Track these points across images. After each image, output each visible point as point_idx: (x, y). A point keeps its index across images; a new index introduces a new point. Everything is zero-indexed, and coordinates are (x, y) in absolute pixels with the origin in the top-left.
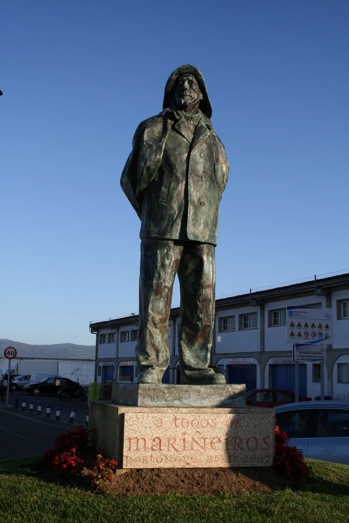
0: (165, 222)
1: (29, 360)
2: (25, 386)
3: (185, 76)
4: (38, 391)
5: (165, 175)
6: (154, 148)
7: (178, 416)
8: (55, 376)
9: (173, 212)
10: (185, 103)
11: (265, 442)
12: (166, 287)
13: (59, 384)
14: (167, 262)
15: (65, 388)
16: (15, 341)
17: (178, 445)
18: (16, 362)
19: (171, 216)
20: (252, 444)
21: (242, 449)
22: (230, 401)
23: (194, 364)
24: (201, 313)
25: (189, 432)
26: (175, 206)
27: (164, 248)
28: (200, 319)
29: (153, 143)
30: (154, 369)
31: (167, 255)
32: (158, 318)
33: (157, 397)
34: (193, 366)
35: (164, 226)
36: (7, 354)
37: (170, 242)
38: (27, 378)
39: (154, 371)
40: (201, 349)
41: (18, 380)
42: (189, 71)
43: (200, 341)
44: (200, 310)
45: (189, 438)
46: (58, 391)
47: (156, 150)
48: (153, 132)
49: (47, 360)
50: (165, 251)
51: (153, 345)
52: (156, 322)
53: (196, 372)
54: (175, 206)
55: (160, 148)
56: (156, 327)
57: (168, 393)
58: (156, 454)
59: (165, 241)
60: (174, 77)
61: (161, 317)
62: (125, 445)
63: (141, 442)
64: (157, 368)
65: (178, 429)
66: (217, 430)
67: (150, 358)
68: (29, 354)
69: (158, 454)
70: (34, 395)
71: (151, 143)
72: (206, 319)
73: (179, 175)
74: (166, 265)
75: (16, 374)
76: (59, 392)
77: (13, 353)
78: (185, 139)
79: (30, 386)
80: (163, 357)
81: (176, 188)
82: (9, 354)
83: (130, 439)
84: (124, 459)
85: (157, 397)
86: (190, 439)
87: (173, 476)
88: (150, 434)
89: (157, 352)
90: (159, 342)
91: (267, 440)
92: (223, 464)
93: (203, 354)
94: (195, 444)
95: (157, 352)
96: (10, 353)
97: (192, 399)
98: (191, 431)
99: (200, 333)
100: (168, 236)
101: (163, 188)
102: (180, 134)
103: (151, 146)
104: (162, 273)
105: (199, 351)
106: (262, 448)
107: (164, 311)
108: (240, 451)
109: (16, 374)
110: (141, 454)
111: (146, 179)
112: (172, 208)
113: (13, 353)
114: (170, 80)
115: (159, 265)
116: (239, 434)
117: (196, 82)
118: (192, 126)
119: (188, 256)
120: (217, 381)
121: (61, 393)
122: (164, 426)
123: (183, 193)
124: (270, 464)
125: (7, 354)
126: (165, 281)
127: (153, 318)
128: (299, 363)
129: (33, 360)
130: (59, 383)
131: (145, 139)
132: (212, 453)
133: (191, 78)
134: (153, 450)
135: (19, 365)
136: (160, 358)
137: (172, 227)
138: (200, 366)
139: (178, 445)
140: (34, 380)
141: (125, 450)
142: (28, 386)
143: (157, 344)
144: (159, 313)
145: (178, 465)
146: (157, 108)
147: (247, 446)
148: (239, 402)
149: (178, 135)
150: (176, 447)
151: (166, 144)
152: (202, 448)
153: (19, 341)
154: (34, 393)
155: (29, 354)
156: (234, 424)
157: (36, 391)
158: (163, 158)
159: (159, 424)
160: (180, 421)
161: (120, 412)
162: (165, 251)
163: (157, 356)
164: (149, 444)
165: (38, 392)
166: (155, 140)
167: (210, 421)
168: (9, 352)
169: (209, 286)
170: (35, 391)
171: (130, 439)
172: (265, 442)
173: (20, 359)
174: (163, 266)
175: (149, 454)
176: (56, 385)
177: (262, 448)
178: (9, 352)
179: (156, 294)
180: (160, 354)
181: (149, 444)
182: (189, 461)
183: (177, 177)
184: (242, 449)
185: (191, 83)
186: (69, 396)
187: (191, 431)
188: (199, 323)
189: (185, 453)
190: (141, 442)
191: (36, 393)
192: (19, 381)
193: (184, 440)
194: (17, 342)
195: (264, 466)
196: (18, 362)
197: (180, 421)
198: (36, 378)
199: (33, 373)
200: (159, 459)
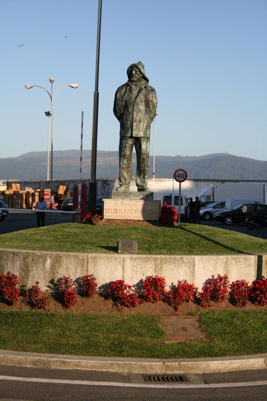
0: (126, 130)
1: (232, 183)
2: (215, 214)
3: (134, 68)
4: (230, 219)
5: (126, 111)
6: (121, 100)
7: (123, 202)
8: (255, 202)
9: (128, 126)
10: (133, 80)
11: (156, 212)
12: (127, 155)
13: (246, 211)
14: (127, 145)
15: (254, 216)
16: (239, 156)
17: (123, 211)
18: (212, 186)
19: (128, 128)
20: (150, 212)
21: (147, 214)
22: (146, 198)
23: (140, 184)
24: (142, 164)
25: (127, 207)
26: (129, 123)
27: (125, 140)
28: (141, 167)
29: (120, 98)
30: (122, 186)
31: (127, 143)
32: (124, 166)
33: (119, 196)
34: (139, 185)
35: (125, 131)
36: (177, 176)
37: (128, 137)
38: (223, 204)
39: (123, 187)
40: (143, 178)
41: (213, 208)
42: (134, 66)
43: (142, 175)
44: (141, 163)
45: (127, 209)
46: (246, 219)
47: (121, 101)
48: (121, 93)
49: (255, 183)
50: (126, 141)
51: (123, 177)
52: (124, 168)
53: (141, 187)
54: (129, 123)
55: (123, 100)
56: (124, 170)
57: (123, 194)
58: (115, 214)
59: (126, 137)
60: (129, 69)
61: (126, 166)
62: (104, 211)
63: (110, 210)
64: (124, 186)
65: (123, 206)
66: (137, 207)
67: (122, 182)
68: (260, 175)
69: (116, 214)
70: (225, 224)
71: (120, 98)
72: (144, 167)
73: (130, 111)
74: (126, 146)
75: (212, 201)
76: (247, 220)
77: (183, 176)
78: (134, 95)
79: (221, 214)
80: (128, 181)
81: (129, 116)
82: (179, 177)
83: (106, 209)
84: (104, 215)
85: (119, 196)
86: (127, 210)
87: (120, 222)
88: (113, 207)
89: (125, 179)
90: (126, 176)
91: (156, 211)
92: (141, 218)
93: (144, 180)
94: (129, 212)
95: (125, 179)
96: (180, 176)
97: (132, 197)
98: (127, 207)
99: (142, 172)
100: (126, 135)
101: (124, 116)
102: (132, 93)
103: (120, 100)
104: (125, 149)
105: (142, 179)
106: (154, 214)
107: (127, 164)
108: (146, 215)
109: (212, 201)
110: (110, 214)
111: (120, 112)
112: (128, 124)
113: (183, 176)
114: (128, 70)
115: (124, 146)
116: (145, 209)
117: (138, 70)
118: (138, 88)
119: (137, 142)
120: (146, 191)
121: (248, 222)
122: (118, 205)
123: (132, 118)
124: (157, 219)
125: (177, 176)
126: (126, 152)
127: (123, 166)
128: (117, 184)
129: (237, 183)
130: (246, 209)
131: (118, 97)
132: (135, 215)
133: (136, 69)
134: (114, 213)
135: (215, 189)
136: (127, 182)
137: (128, 132)
138: (142, 185)
139: (123, 211)
140: (229, 207)
141: (104, 213)
142: (218, 214)
143: (124, 176)
144: (125, 165)
145: (123, 218)
146: (125, 80)
147: (149, 213)
148: (150, 198)
149: (131, 94)
150: (122, 212)
151: (126, 98)
152: (132, 213)
153: (244, 156)
154: (226, 222)
155: (260, 175)
156: (144, 205)
157: (229, 220)
158: (125, 103)
159: (116, 205)
160: (123, 204)
161: (103, 200)
162: (126, 141)
163: (125, 181)
164: (113, 211)
165: (230, 222)
166: (122, 97)
167: (135, 204)
168: (179, 174)
169: (144, 154)
170: (227, 220)
171: (106, 209)
172: (156, 212)
173: (220, 182)
174: (125, 147)
175: (112, 214)
176: (244, 211)
177: (154, 214)
178: (179, 174)
179: (123, 158)
180: (126, 180)
181: (113, 211)
182: (127, 217)
183: (129, 112)
184: (147, 214)
185: (136, 71)
186: (258, 225)
187: (127, 207)
188: (141, 168)
189: (125, 214)
190: (110, 210)
191: (228, 222)
192: (214, 209)
193: (125, 210)
194: (241, 158)
195: (155, 220)
196: (213, 186)
197: (123, 204)
198: (231, 205)
199: (228, 199)
200: (116, 216)
